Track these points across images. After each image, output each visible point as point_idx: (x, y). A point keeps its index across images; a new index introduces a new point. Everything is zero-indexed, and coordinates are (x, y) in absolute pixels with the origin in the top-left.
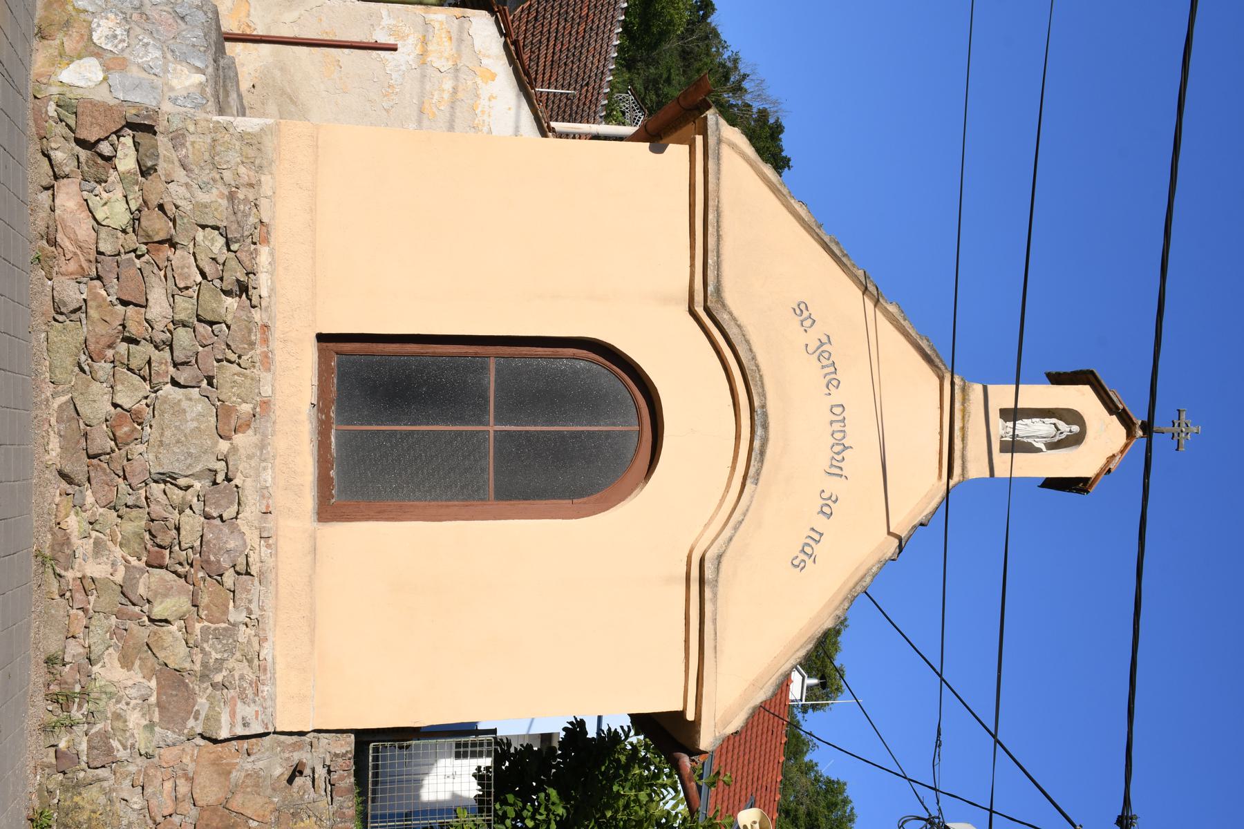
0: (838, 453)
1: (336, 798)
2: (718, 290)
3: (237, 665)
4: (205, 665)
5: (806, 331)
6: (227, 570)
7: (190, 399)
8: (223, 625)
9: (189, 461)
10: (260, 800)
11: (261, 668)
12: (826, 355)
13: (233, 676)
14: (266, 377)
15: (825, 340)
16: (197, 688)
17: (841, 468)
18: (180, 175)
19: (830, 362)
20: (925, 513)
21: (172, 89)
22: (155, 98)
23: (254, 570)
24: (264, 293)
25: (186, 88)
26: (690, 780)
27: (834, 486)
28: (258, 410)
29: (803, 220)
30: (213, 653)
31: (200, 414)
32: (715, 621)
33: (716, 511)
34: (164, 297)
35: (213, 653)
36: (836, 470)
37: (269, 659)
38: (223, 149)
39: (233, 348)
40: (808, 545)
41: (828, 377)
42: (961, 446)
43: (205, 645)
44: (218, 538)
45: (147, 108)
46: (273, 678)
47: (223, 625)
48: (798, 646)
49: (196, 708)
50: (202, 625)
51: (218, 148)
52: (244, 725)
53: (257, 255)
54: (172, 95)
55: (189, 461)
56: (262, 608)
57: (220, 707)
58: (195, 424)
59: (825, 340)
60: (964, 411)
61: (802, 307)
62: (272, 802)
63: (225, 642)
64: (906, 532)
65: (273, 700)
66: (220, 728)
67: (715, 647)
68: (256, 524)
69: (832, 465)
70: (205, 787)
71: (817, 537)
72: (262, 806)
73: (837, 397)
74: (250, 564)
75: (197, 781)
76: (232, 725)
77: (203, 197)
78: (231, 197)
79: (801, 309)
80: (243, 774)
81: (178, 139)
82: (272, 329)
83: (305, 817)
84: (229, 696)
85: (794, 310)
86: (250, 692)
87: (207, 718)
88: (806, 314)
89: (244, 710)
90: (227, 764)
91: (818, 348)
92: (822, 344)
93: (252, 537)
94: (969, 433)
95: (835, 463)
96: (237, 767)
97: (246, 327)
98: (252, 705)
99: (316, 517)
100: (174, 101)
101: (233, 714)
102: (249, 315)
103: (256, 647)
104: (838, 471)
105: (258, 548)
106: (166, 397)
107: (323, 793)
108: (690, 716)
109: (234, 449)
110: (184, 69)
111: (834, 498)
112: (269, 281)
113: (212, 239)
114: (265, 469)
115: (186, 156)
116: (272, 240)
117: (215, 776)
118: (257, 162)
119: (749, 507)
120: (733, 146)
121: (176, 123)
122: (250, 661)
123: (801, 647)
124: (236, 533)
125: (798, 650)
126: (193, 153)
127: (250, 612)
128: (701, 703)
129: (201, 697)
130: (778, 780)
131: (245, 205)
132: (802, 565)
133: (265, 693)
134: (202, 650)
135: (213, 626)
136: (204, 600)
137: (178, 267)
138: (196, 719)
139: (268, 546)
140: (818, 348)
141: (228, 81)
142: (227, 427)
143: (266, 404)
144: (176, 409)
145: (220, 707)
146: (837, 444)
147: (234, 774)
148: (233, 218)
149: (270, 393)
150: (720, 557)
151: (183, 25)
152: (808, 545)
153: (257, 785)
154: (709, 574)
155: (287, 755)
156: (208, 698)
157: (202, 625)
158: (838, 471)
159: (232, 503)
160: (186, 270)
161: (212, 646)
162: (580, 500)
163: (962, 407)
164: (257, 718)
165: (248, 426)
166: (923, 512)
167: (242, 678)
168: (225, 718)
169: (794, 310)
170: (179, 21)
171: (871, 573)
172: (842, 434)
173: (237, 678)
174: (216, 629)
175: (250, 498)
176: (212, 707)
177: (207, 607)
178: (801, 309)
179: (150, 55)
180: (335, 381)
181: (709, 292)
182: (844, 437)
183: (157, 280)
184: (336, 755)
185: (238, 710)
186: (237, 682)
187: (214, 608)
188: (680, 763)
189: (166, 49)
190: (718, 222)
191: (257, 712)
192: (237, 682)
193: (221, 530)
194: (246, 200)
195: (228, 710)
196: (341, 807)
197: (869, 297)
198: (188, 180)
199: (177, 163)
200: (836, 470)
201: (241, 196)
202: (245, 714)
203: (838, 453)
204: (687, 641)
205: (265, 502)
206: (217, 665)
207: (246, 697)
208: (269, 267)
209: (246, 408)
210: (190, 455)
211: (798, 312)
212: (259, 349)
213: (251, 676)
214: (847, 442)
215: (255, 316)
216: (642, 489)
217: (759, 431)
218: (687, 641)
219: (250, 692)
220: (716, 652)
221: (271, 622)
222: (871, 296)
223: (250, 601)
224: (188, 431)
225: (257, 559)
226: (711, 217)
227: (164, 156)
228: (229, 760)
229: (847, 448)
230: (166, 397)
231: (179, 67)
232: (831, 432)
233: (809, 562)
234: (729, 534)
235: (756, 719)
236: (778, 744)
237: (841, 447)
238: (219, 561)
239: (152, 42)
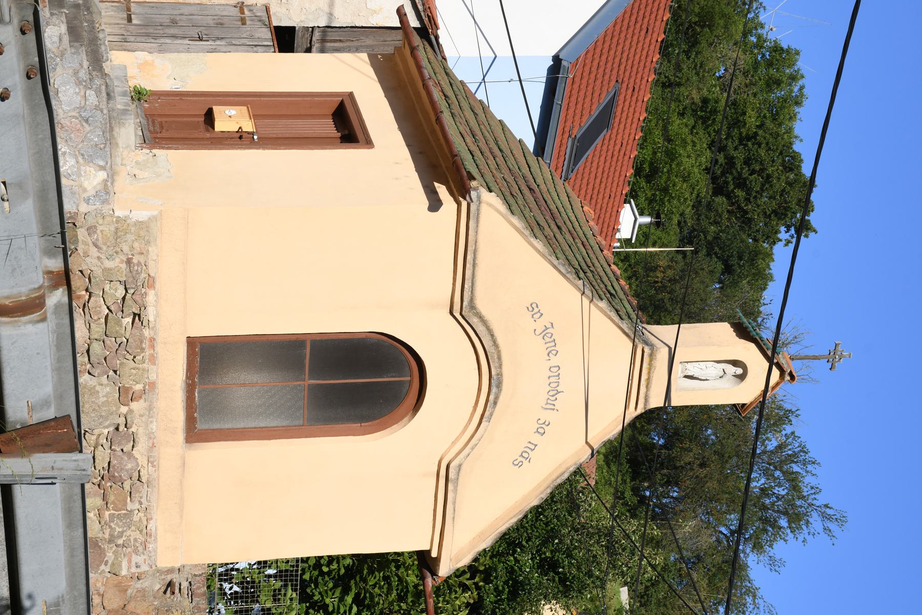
0: (553, 396)
1: (194, 599)
2: (472, 300)
3: (133, 534)
4: (111, 535)
5: (535, 321)
6: (126, 480)
7: (102, 385)
8: (123, 512)
9: (101, 420)
10: (146, 604)
11: (148, 534)
12: (549, 335)
13: (130, 540)
14: (152, 368)
15: (549, 325)
16: (106, 547)
17: (554, 405)
18: (93, 251)
19: (552, 339)
20: (613, 434)
21: (85, 190)
22: (74, 203)
23: (144, 479)
24: (151, 319)
25: (95, 187)
26: (430, 598)
27: (547, 416)
28: (147, 387)
29: (539, 251)
30: (117, 528)
31: (108, 393)
32: (454, 503)
33: (460, 434)
34: (84, 325)
35: (117, 528)
36: (550, 406)
37: (153, 529)
38: (122, 234)
39: (130, 352)
40: (526, 452)
41: (549, 349)
42: (645, 391)
43: (112, 524)
44: (121, 463)
45: (70, 212)
46: (155, 540)
47: (123, 512)
48: (512, 516)
49: (106, 559)
50: (109, 512)
51: (119, 234)
52: (137, 567)
53: (146, 296)
54: (85, 195)
55: (101, 420)
56: (149, 501)
57: (121, 558)
58: (105, 399)
59: (549, 325)
60: (650, 364)
61: (534, 306)
62: (153, 605)
63: (124, 521)
64: (597, 446)
65: (155, 551)
66: (122, 570)
67: (454, 518)
68: (145, 453)
69: (547, 403)
70: (111, 599)
71: (532, 447)
72: (147, 607)
73: (555, 361)
74: (141, 476)
75: (105, 596)
76: (129, 568)
77: (109, 264)
78: (129, 262)
79: (534, 309)
80: (135, 591)
81: (91, 230)
82: (157, 340)
83: (174, 611)
84: (127, 552)
85: (528, 308)
86: (140, 549)
87: (113, 564)
88: (536, 310)
89: (135, 559)
90: (125, 586)
91: (544, 331)
92: (547, 329)
93: (142, 461)
94: (653, 382)
95: (549, 401)
96: (131, 587)
97: (139, 339)
98: (142, 555)
99: (184, 441)
100: (87, 201)
101: (130, 561)
102: (141, 332)
103: (145, 523)
104: (552, 407)
105: (146, 466)
106: (86, 385)
107: (186, 596)
108: (434, 554)
109: (131, 411)
110: (91, 169)
111: (547, 423)
112: (155, 312)
113: (116, 289)
114: (151, 422)
115: (97, 239)
116: (157, 285)
117: (117, 593)
118: (146, 238)
119: (483, 435)
120: (490, 205)
121: (91, 221)
122: (141, 531)
123: (514, 516)
124: (132, 459)
125: (511, 518)
126: (102, 237)
127: (141, 503)
128: (441, 549)
129: (109, 553)
130: (660, 40)
131: (138, 266)
132: (520, 464)
133: (150, 549)
134: (110, 527)
135: (117, 513)
136: (111, 498)
137: (93, 308)
138: (106, 565)
139: (153, 466)
140: (544, 331)
141: (112, 120)
142: (126, 399)
143: (153, 385)
144: (92, 391)
145: (121, 558)
146: (552, 390)
147: (129, 591)
148: (130, 275)
149: (155, 378)
150: (460, 466)
151: (87, 128)
152: (526, 452)
153: (144, 596)
154: (452, 476)
155: (163, 577)
156: (113, 553)
157: (109, 512)
158: (552, 407)
159: (129, 442)
160: (98, 309)
161: (117, 524)
162: (366, 424)
163: (648, 366)
164: (145, 562)
165: (141, 397)
166: (612, 431)
167: (135, 540)
168: (125, 564)
169: (528, 308)
170: (84, 124)
171: (568, 471)
172: (557, 384)
173: (132, 541)
174: (119, 514)
175: (141, 439)
176: (116, 558)
177: (113, 503)
178: (534, 309)
179: (68, 163)
180: (198, 360)
181: (464, 306)
182: (558, 386)
183: (79, 315)
184: (195, 575)
185: (133, 559)
186: (132, 543)
187: (118, 502)
188: (426, 580)
189: (77, 153)
190: (472, 292)
191: (145, 559)
192: (132, 543)
193: (122, 458)
194: (139, 264)
195: (126, 559)
196: (198, 604)
197: (585, 297)
198: (99, 254)
199: (91, 244)
200: (550, 406)
201: (135, 261)
202: (137, 561)
203: (553, 396)
204: (435, 511)
205: (151, 441)
206: (120, 534)
207: (138, 551)
208: (154, 303)
209: (139, 387)
210: (102, 416)
211: (530, 309)
212: (148, 352)
213: (141, 538)
214: (559, 389)
215: (145, 333)
216: (410, 421)
217: (494, 390)
218: (435, 511)
219: (140, 549)
220: (454, 521)
221: (155, 508)
222: (587, 297)
223: (141, 498)
224: (100, 403)
225: (146, 473)
226: (469, 257)
227: (82, 241)
228: (126, 584)
229: (559, 392)
230: (86, 385)
231: (88, 169)
232: (548, 383)
233: (526, 462)
234: (468, 452)
235: (618, 27)
236: (653, 41)
237: (556, 392)
238: (121, 476)
239: (68, 151)
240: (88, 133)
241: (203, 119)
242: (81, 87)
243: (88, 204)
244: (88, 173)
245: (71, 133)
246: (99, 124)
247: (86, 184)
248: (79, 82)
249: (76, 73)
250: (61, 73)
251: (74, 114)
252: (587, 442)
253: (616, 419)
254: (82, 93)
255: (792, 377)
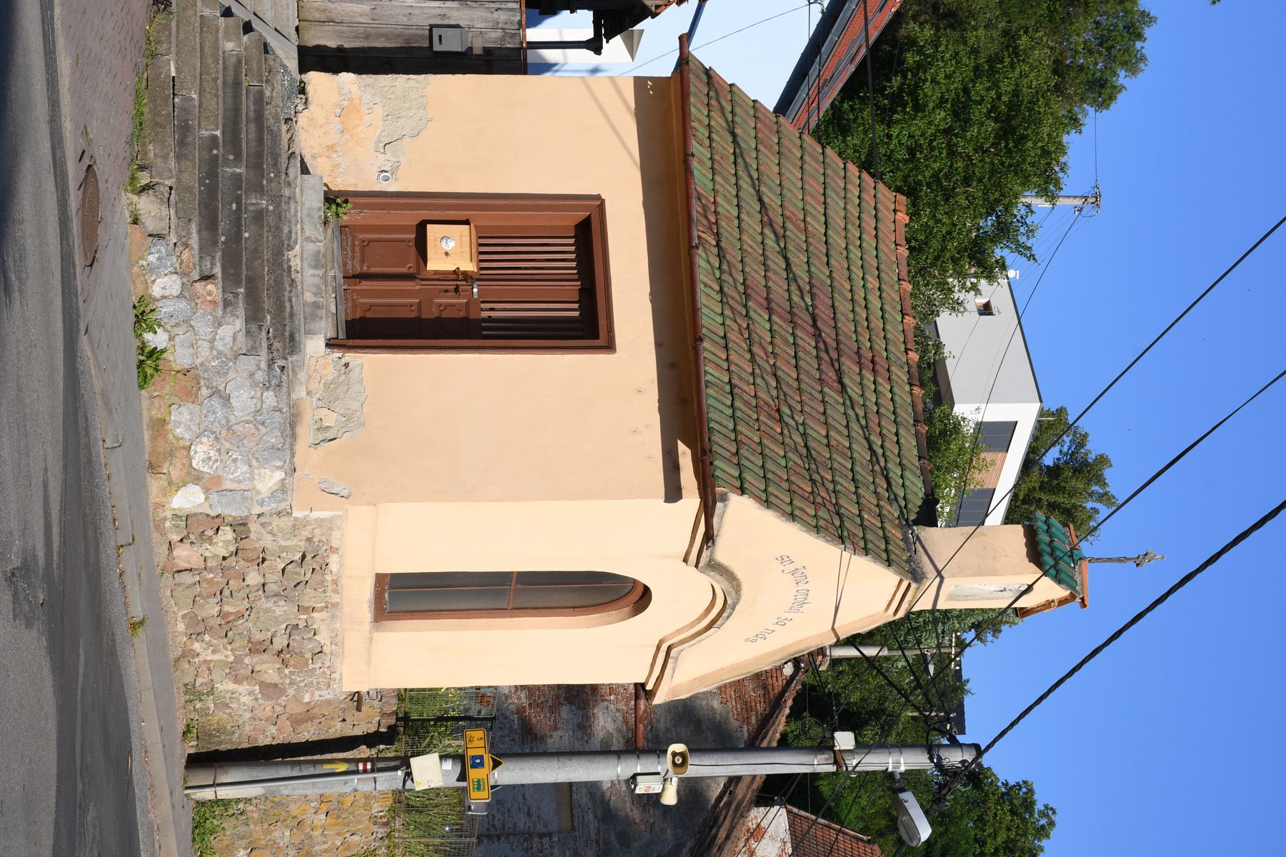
21: (258, 492)
25: (270, 488)
33: (687, 626)
54: (259, 498)
100: (261, 504)
151: (263, 430)
170: (260, 427)
189: (250, 456)
231: (263, 471)
240: (264, 435)
241: (414, 236)
242: (257, 389)
243: (262, 506)
244: (263, 475)
245: (244, 439)
246: (277, 425)
247: (260, 486)
248: (254, 385)
249: (251, 375)
250: (234, 376)
251: (248, 418)
252: (833, 629)
253: (870, 616)
254: (259, 394)
255: (1083, 604)
